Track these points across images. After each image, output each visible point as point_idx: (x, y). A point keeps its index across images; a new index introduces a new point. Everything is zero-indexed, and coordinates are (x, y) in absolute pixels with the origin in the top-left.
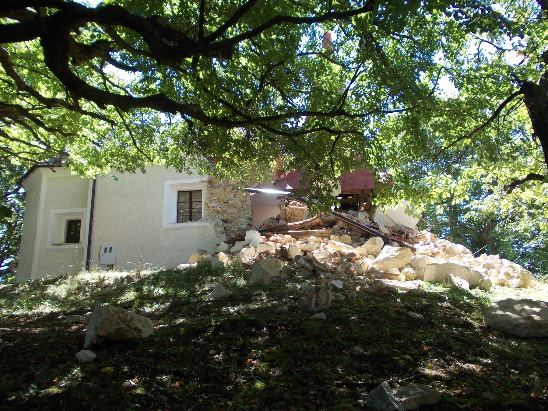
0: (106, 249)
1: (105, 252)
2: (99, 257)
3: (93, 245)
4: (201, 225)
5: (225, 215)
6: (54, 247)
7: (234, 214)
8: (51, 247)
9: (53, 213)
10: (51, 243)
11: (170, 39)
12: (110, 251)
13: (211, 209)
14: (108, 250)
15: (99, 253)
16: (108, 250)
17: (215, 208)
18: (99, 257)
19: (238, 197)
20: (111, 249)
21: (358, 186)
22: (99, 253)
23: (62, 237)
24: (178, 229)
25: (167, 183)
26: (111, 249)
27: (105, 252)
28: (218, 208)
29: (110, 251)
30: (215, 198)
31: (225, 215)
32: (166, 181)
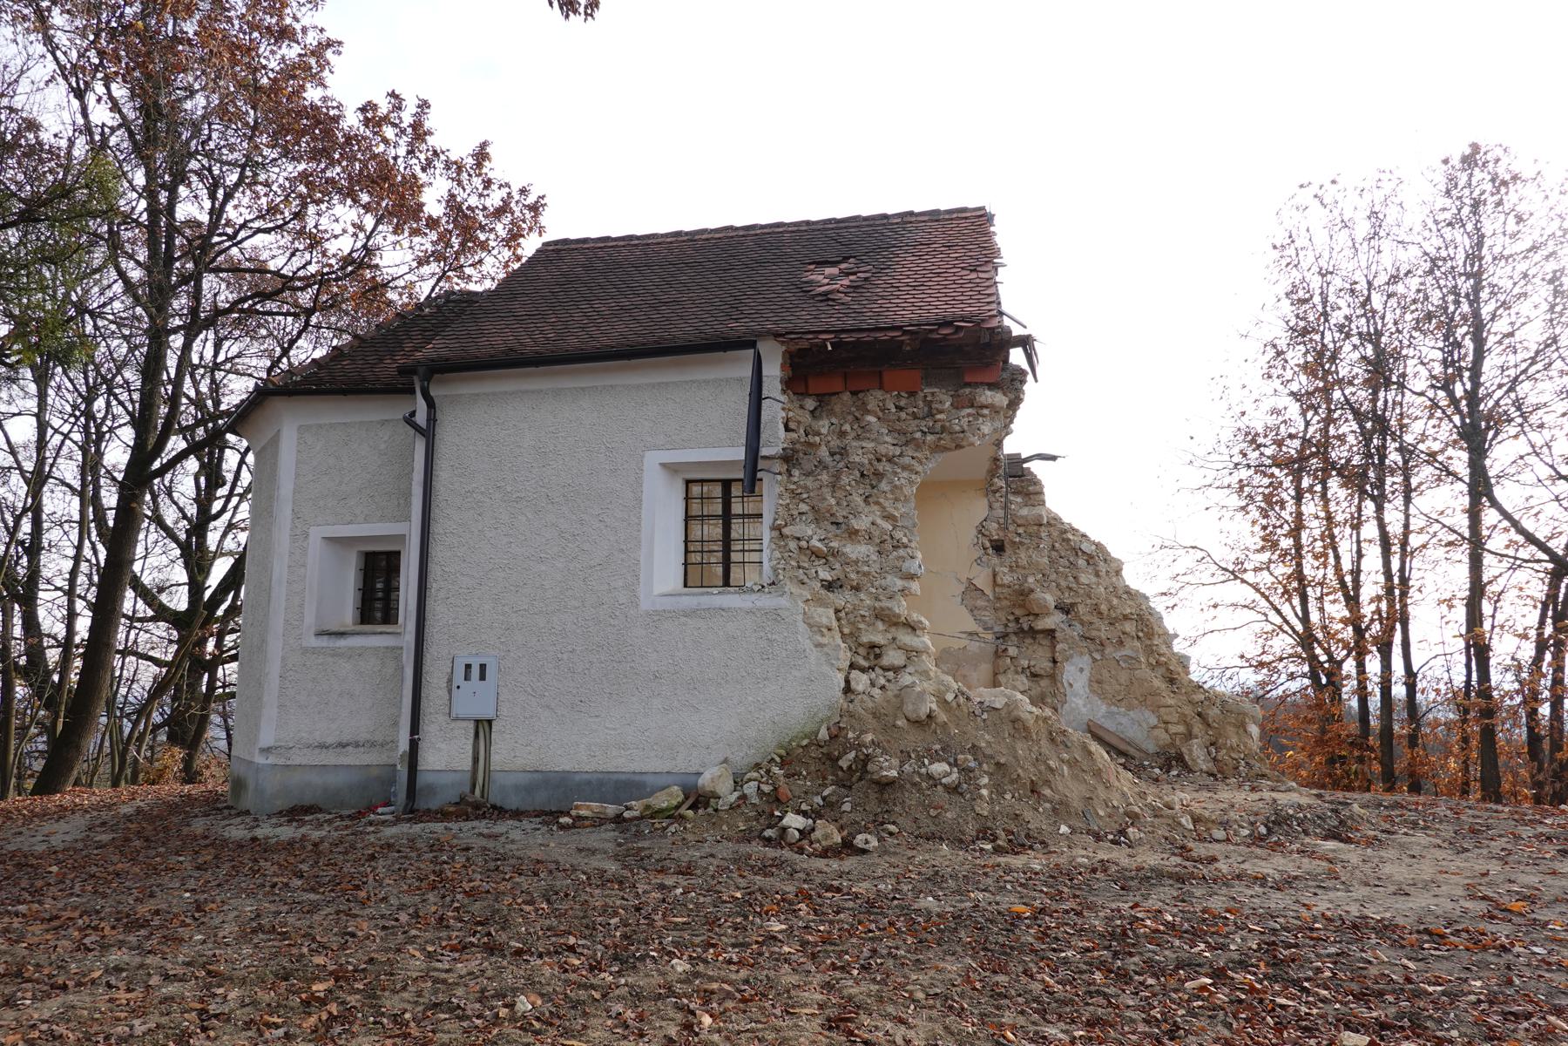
0: (468, 667)
1: (467, 678)
2: (450, 692)
3: (432, 652)
4: (759, 604)
5: (837, 566)
6: (324, 642)
7: (866, 563)
8: (314, 642)
9: (317, 533)
10: (313, 631)
11: (374, 590)
12: (483, 677)
13: (793, 545)
14: (475, 672)
15: (450, 681)
16: (475, 672)
17: (804, 544)
18: (450, 692)
19: (877, 503)
20: (483, 667)
21: (1085, 727)
22: (450, 681)
23: (346, 610)
24: (691, 613)
25: (653, 459)
26: (483, 667)
27: (467, 678)
28: (815, 543)
29: (483, 677)
30: (804, 507)
31: (837, 566)
32: (648, 454)
